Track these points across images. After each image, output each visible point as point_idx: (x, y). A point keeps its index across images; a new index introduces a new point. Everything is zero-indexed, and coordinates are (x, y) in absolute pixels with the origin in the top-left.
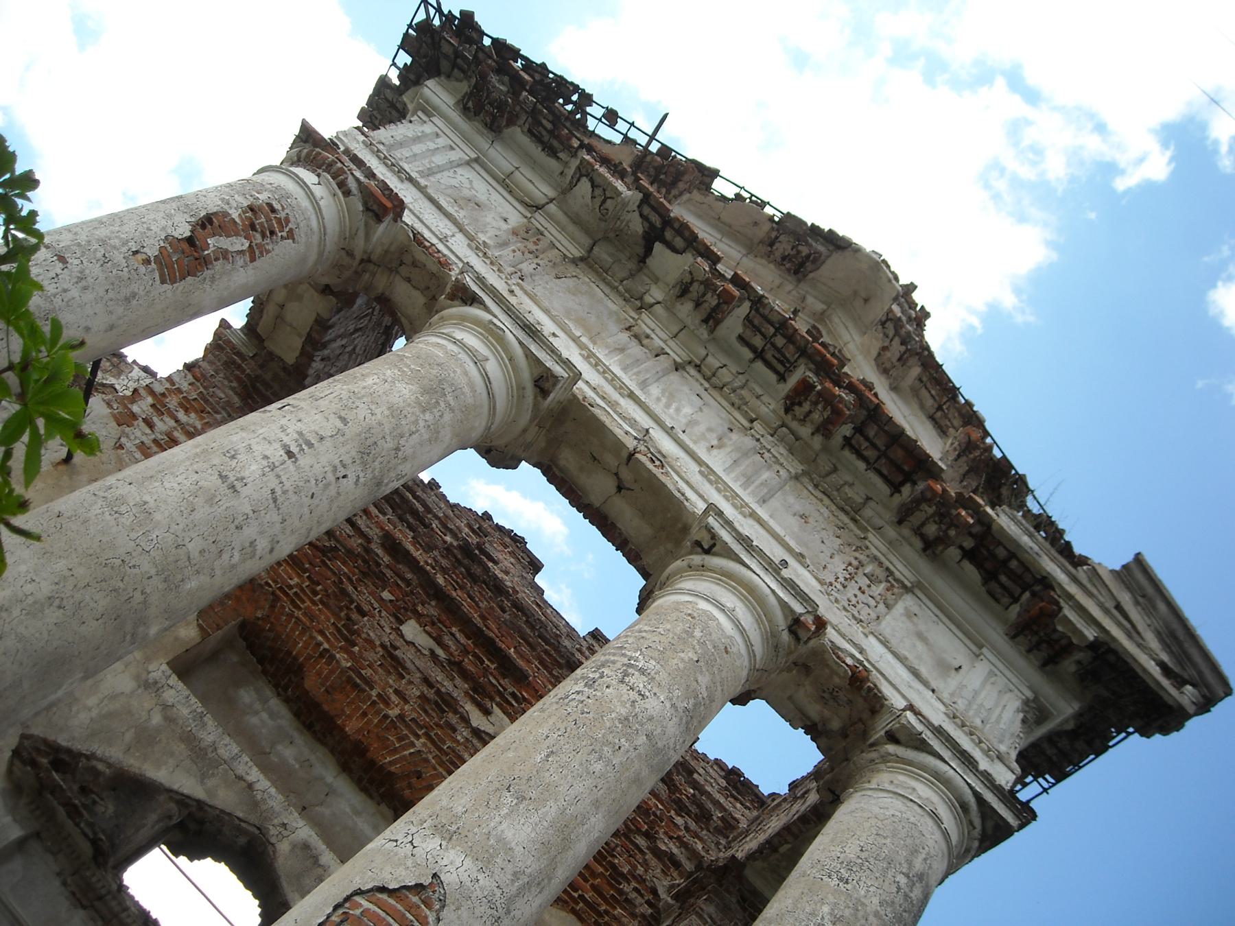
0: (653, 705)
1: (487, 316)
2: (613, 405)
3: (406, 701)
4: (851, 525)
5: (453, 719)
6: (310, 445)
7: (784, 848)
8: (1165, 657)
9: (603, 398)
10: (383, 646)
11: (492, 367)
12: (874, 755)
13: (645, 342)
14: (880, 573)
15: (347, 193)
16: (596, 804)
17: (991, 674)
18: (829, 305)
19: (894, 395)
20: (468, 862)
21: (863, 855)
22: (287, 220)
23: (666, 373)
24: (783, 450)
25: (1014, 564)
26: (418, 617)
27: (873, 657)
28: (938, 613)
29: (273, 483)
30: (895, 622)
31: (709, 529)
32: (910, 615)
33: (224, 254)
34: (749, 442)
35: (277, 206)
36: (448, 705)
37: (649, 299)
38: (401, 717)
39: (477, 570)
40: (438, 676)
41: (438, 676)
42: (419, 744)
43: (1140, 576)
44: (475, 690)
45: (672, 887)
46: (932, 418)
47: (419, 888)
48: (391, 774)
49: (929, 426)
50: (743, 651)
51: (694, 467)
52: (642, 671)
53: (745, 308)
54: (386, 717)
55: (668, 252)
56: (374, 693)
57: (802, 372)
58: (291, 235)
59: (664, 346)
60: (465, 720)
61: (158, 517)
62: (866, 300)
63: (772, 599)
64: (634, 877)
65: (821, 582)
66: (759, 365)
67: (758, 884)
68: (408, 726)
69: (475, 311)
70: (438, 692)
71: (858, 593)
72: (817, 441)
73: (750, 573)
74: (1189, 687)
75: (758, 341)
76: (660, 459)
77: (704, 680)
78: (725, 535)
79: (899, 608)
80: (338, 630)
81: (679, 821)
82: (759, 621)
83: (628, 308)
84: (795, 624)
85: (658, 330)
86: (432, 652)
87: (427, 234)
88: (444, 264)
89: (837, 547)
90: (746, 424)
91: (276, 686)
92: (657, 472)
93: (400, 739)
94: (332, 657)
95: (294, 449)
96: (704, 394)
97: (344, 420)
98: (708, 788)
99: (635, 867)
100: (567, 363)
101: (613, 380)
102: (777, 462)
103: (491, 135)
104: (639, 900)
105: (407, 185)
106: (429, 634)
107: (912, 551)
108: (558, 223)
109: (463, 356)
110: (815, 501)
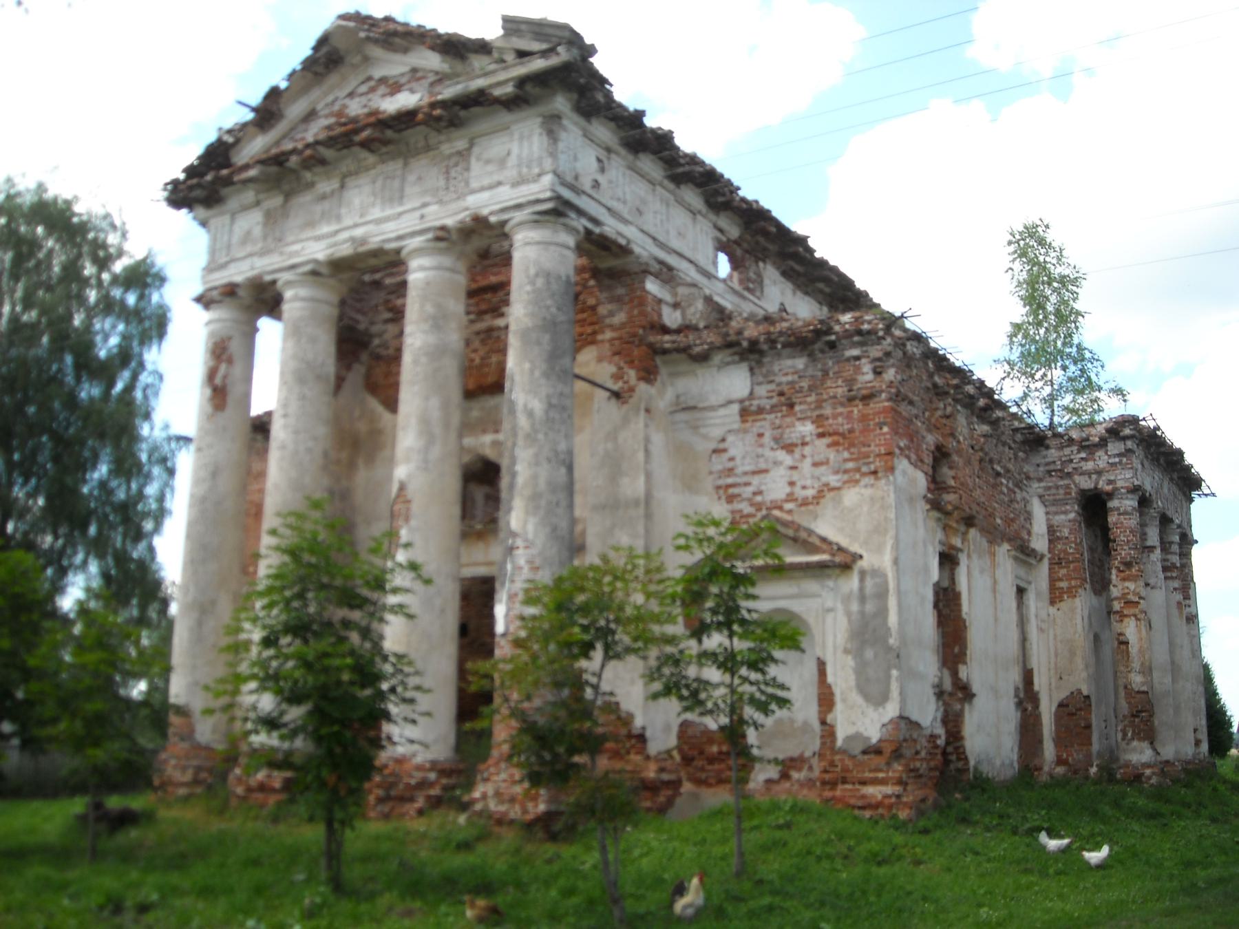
30: (478, 172)
33: (225, 377)
58: (230, 338)
76: (363, 241)
84: (438, 239)
107: (456, 133)
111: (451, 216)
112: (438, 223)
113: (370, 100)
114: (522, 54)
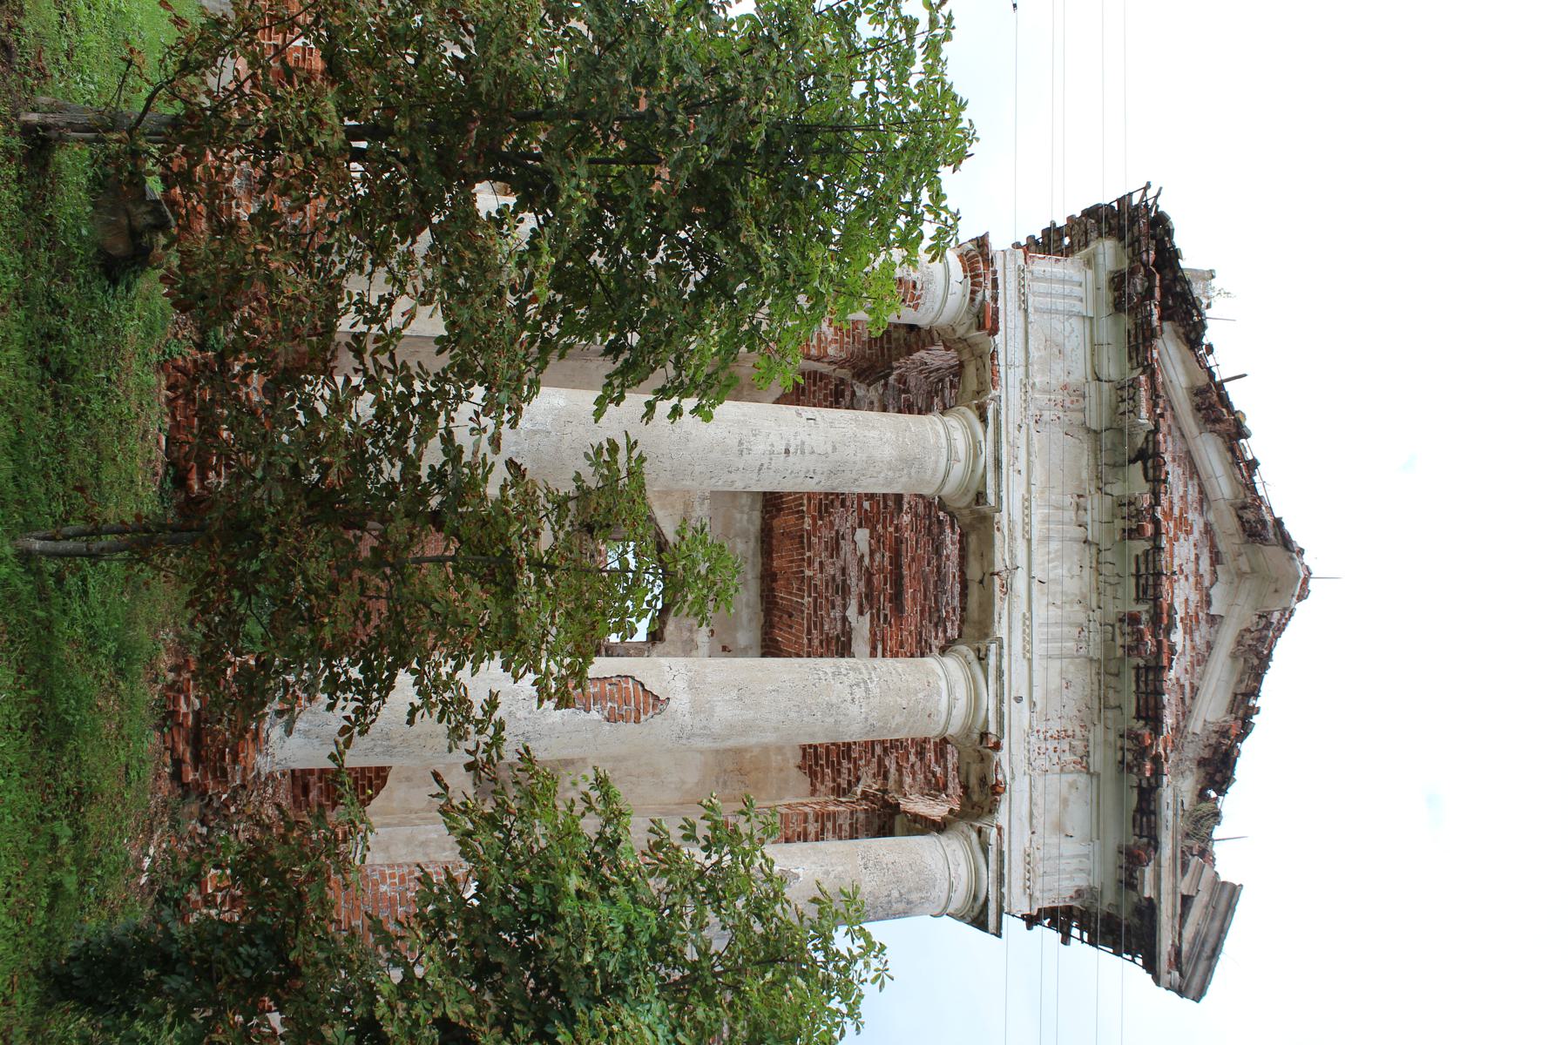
0: (854, 710)
1: (981, 437)
2: (1012, 538)
3: (821, 572)
4: (1097, 711)
5: (839, 601)
6: (803, 452)
7: (918, 826)
8: (1185, 947)
9: (1010, 530)
10: (837, 532)
11: (958, 469)
12: (966, 830)
13: (1081, 512)
14: (1080, 750)
15: (972, 300)
16: (776, 729)
17: (1087, 856)
18: (1253, 571)
19: (1229, 661)
20: (688, 705)
21: (890, 866)
22: (919, 297)
23: (1075, 540)
24: (1098, 638)
25: (1153, 818)
26: (873, 530)
27: (1015, 786)
28: (1095, 800)
29: (766, 461)
31: (987, 649)
32: (1072, 785)
34: (1081, 617)
35: (919, 286)
36: (843, 592)
37: (1108, 489)
38: (810, 578)
39: (935, 530)
40: (853, 571)
41: (853, 571)
42: (806, 599)
43: (1225, 896)
44: (866, 596)
45: (870, 787)
46: (1235, 695)
47: (656, 698)
48: (777, 603)
49: (1229, 697)
50: (942, 722)
51: (1024, 608)
52: (867, 690)
53: (1147, 545)
54: (802, 572)
55: (1141, 473)
56: (808, 554)
57: (1143, 607)
58: (916, 307)
59: (1090, 522)
60: (845, 607)
61: (691, 445)
62: (1276, 591)
63: (983, 713)
64: (855, 763)
65: (1031, 727)
66: (1133, 581)
67: (898, 828)
68: (809, 586)
69: (978, 427)
70: (844, 581)
71: (1051, 749)
72: (1119, 652)
73: (985, 690)
74: (1177, 974)
75: (1143, 570)
76: (1007, 589)
77: (899, 719)
78: (992, 660)
79: (1071, 778)
80: (820, 503)
81: (912, 758)
82: (967, 716)
83: (1094, 483)
84: (984, 735)
85: (1095, 512)
86: (862, 556)
87: (1001, 356)
88: (994, 384)
89: (1071, 715)
90: (1094, 606)
91: (764, 506)
92: (998, 594)
93: (799, 589)
94: (803, 517)
95: (792, 450)
96: (1086, 571)
97: (834, 449)
98: (949, 757)
99: (861, 758)
100: (999, 498)
101: (1027, 524)
102: (1088, 642)
103: (1112, 310)
104: (846, 776)
105: (1021, 313)
106: (870, 544)
108: (1101, 398)
109: (944, 452)
110: (1088, 680)
111: (1012, 762)
112: (1005, 742)
113: (1187, 578)
114: (1186, 901)
